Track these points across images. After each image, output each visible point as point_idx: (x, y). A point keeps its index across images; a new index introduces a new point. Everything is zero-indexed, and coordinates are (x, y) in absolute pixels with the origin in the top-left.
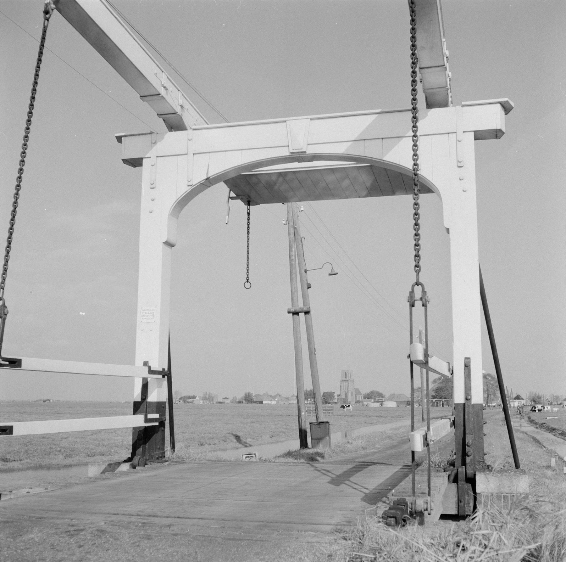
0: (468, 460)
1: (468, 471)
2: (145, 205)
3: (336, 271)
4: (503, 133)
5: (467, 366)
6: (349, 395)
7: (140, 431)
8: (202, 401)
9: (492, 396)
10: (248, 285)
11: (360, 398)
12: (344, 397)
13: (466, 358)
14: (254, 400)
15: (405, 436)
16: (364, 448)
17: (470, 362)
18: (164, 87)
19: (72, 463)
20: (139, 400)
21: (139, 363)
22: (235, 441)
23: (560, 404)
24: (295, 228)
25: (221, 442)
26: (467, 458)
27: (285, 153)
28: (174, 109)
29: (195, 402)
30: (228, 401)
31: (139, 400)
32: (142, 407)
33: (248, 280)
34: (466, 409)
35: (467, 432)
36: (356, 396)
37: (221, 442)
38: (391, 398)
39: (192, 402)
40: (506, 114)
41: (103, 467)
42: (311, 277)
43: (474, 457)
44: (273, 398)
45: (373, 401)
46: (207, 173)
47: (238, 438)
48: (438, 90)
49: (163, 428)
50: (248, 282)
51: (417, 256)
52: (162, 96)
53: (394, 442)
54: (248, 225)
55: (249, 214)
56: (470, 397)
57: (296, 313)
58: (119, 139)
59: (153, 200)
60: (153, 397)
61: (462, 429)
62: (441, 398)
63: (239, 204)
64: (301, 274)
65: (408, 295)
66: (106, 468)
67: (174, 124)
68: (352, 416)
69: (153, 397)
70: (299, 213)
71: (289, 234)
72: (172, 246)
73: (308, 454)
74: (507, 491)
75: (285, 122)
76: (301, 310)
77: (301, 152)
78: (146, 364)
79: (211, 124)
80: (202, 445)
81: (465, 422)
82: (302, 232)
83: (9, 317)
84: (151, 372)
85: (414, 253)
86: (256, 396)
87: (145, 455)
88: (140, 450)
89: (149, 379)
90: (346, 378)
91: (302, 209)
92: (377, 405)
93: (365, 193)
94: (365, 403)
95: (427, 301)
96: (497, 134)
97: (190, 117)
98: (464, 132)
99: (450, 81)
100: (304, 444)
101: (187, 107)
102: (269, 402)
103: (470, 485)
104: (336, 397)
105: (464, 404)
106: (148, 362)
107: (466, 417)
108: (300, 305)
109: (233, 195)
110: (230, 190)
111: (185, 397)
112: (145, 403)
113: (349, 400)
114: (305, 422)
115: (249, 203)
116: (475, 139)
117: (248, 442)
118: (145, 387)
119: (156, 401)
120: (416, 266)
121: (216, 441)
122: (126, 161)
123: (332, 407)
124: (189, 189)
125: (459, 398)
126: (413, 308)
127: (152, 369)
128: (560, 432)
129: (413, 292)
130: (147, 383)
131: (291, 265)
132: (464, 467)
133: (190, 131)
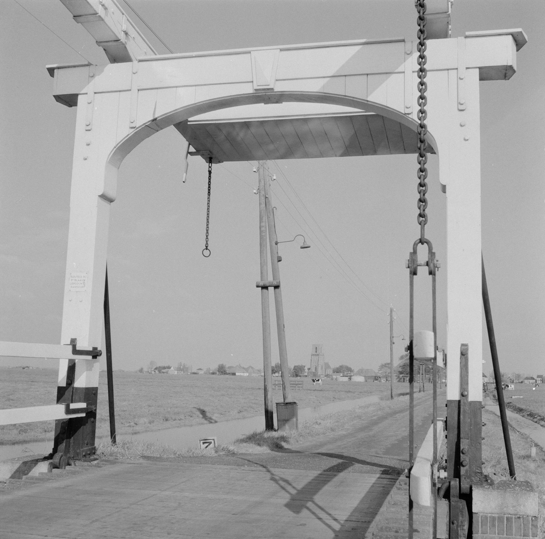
0: (463, 470)
1: (462, 486)
2: (79, 150)
3: (308, 244)
4: (514, 71)
5: (464, 354)
7: (64, 423)
8: (176, 372)
10: (206, 253)
11: (330, 372)
12: (314, 371)
13: (463, 345)
14: (227, 372)
15: (374, 416)
16: (332, 430)
17: (467, 349)
18: (103, 5)
19: (26, 439)
20: (64, 385)
22: (201, 416)
23: (522, 382)
24: (266, 198)
25: (187, 417)
26: (462, 468)
27: (248, 89)
28: (117, 36)
29: (169, 372)
30: (201, 372)
31: (64, 385)
32: (68, 394)
33: (207, 247)
34: (462, 407)
35: (462, 436)
37: (187, 417)
38: (360, 373)
39: (167, 373)
40: (517, 50)
41: (17, 466)
42: (282, 250)
43: (470, 467)
44: (246, 370)
45: (342, 375)
46: (154, 114)
47: (203, 412)
48: (438, 16)
49: (92, 419)
50: (207, 249)
51: (422, 201)
52: (100, 16)
53: (363, 422)
54: (209, 185)
55: (210, 172)
56: (466, 393)
57: (265, 287)
58: (51, 71)
59: (88, 145)
60: (80, 382)
61: (456, 432)
63: (200, 161)
64: (271, 246)
65: (408, 257)
66: (19, 468)
67: (118, 55)
68: (321, 390)
69: (80, 382)
70: (271, 182)
71: (260, 204)
73: (273, 438)
74: (512, 512)
75: (249, 52)
76: (270, 284)
77: (268, 89)
78: (73, 342)
79: (159, 54)
80: (167, 420)
81: (459, 422)
82: (274, 202)
85: (418, 196)
86: (229, 368)
87: (69, 452)
88: (62, 446)
89: (76, 361)
90: (316, 352)
91: (275, 178)
92: (346, 379)
93: (341, 152)
94: (334, 377)
95: (435, 267)
96: (506, 72)
97: (136, 47)
98: (467, 68)
99: (451, 5)
100: (269, 426)
101: (133, 36)
102: (242, 374)
103: (464, 502)
104: (306, 370)
105: (459, 401)
106: (76, 339)
107: (461, 417)
108: (270, 279)
109: (192, 149)
110: (189, 144)
111: (160, 367)
112: (70, 389)
114: (271, 402)
115: (210, 160)
116: (480, 80)
117: (214, 418)
118: (72, 369)
119: (84, 386)
120: (420, 215)
121: (182, 417)
122: (59, 98)
123: (302, 381)
125: (453, 394)
126: (415, 276)
127: (77, 349)
128: (529, 413)
129: (415, 252)
130: (75, 364)
132: (458, 479)
133: (135, 62)
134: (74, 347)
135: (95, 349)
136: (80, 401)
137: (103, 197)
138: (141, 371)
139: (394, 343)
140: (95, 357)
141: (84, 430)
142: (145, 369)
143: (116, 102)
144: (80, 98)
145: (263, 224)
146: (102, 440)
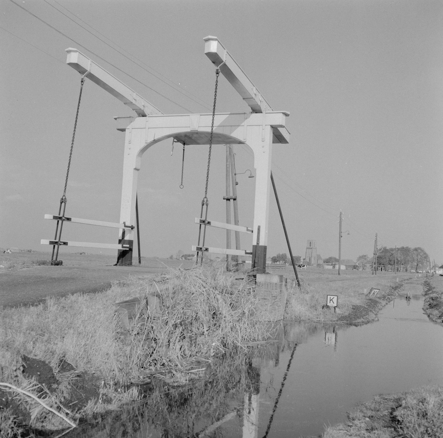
2: (126, 151)
6: (313, 259)
9: (420, 265)
21: (121, 222)
36: (317, 260)
39: (191, 259)
42: (238, 178)
55: (184, 150)
57: (228, 200)
58: (116, 119)
60: (127, 238)
62: (380, 264)
63: (180, 145)
69: (127, 238)
71: (227, 152)
72: (138, 170)
78: (124, 223)
83: (67, 202)
84: (125, 226)
88: (120, 261)
90: (310, 246)
92: (331, 267)
104: (302, 260)
108: (231, 195)
109: (175, 140)
111: (186, 255)
113: (312, 263)
115: (184, 144)
124: (146, 144)
125: (255, 243)
131: (227, 171)
134: (125, 224)
135: (132, 226)
136: (127, 244)
137: (136, 169)
138: (171, 257)
139: (342, 237)
140: (132, 229)
141: (128, 255)
142: (175, 257)
143: (139, 134)
144: (126, 130)
145: (228, 163)
146: (135, 260)
